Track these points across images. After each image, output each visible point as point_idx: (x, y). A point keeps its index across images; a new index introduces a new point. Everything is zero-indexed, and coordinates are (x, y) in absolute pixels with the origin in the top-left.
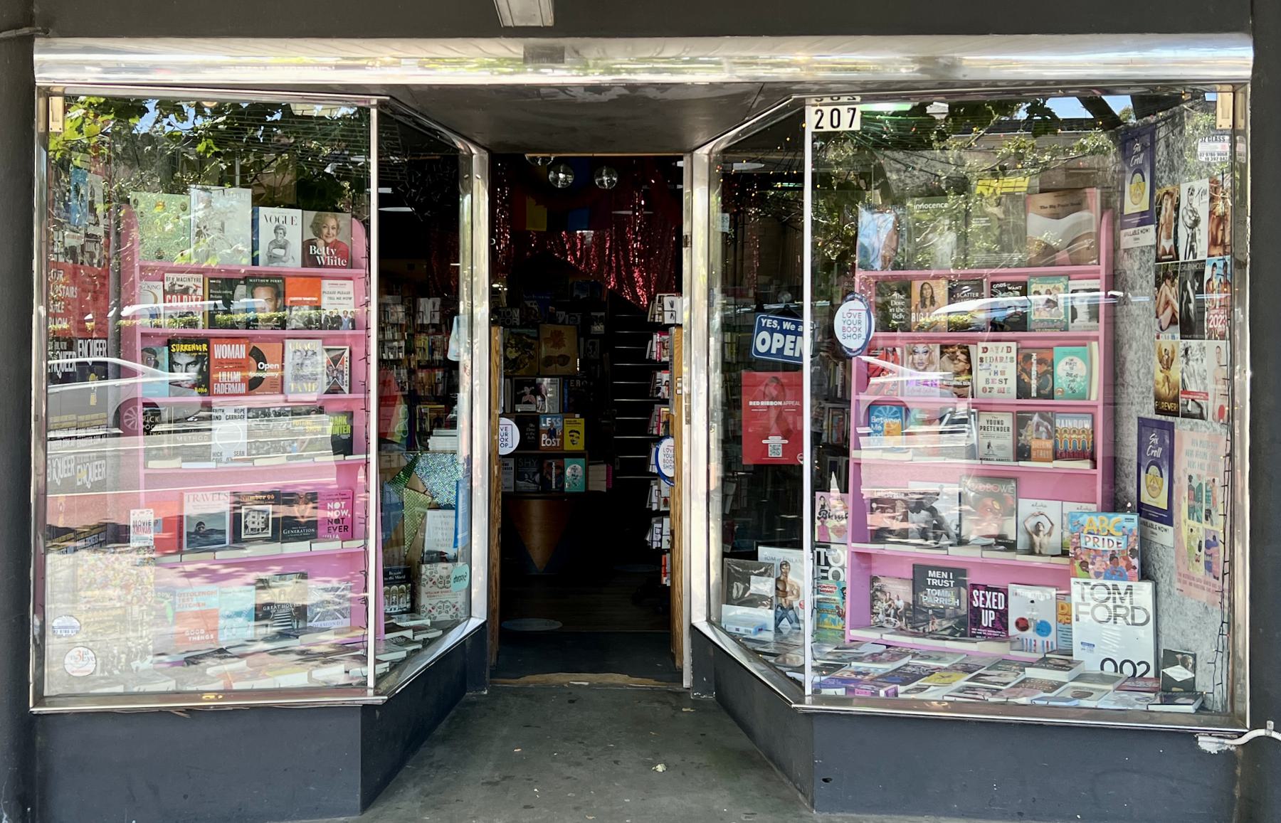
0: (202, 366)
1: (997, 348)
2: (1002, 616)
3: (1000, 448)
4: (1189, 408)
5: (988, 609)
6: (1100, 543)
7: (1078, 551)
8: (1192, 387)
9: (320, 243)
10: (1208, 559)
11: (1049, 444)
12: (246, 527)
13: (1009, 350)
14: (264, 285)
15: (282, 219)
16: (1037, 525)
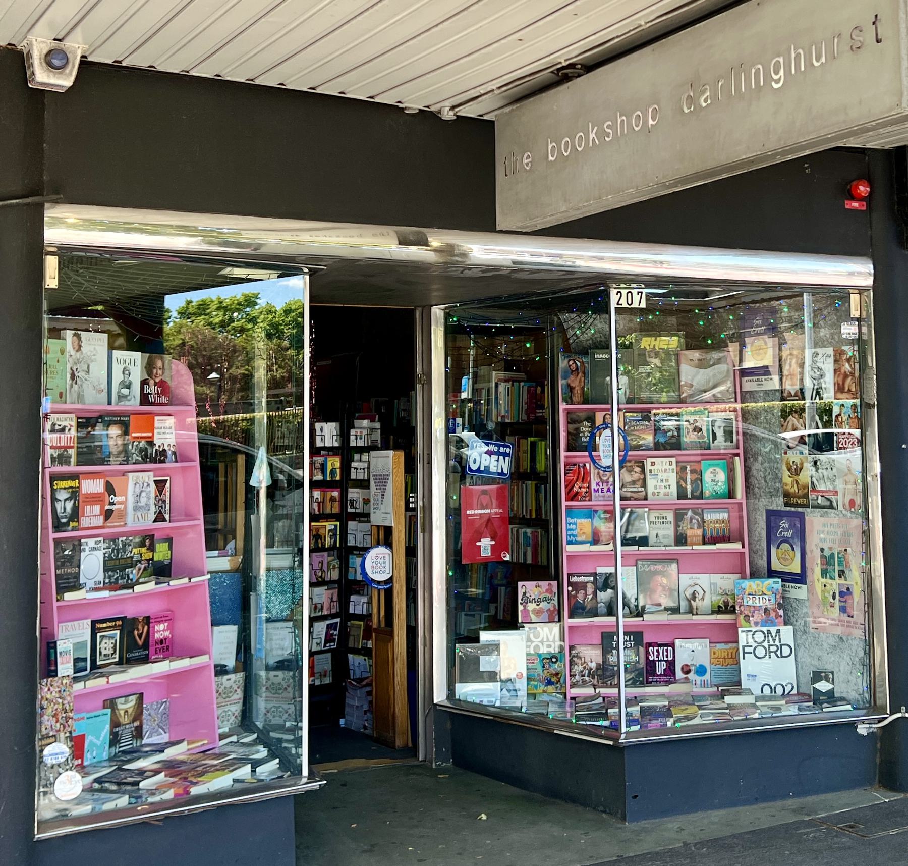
0: (75, 502)
1: (662, 462)
2: (671, 664)
3: (664, 537)
4: (819, 501)
5: (661, 661)
6: (757, 601)
7: (742, 608)
8: (821, 487)
9: (152, 382)
10: (843, 604)
11: (699, 532)
12: (100, 653)
13: (671, 463)
14: (115, 423)
15: (128, 362)
16: (694, 593)
